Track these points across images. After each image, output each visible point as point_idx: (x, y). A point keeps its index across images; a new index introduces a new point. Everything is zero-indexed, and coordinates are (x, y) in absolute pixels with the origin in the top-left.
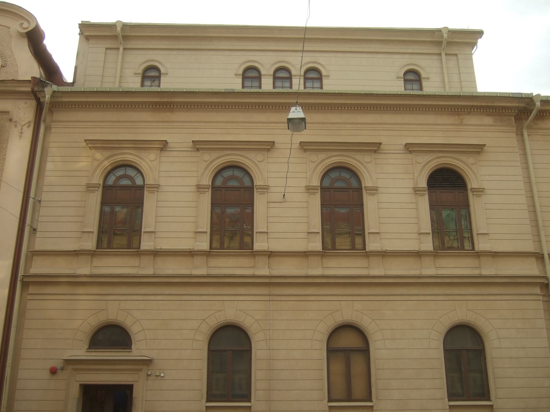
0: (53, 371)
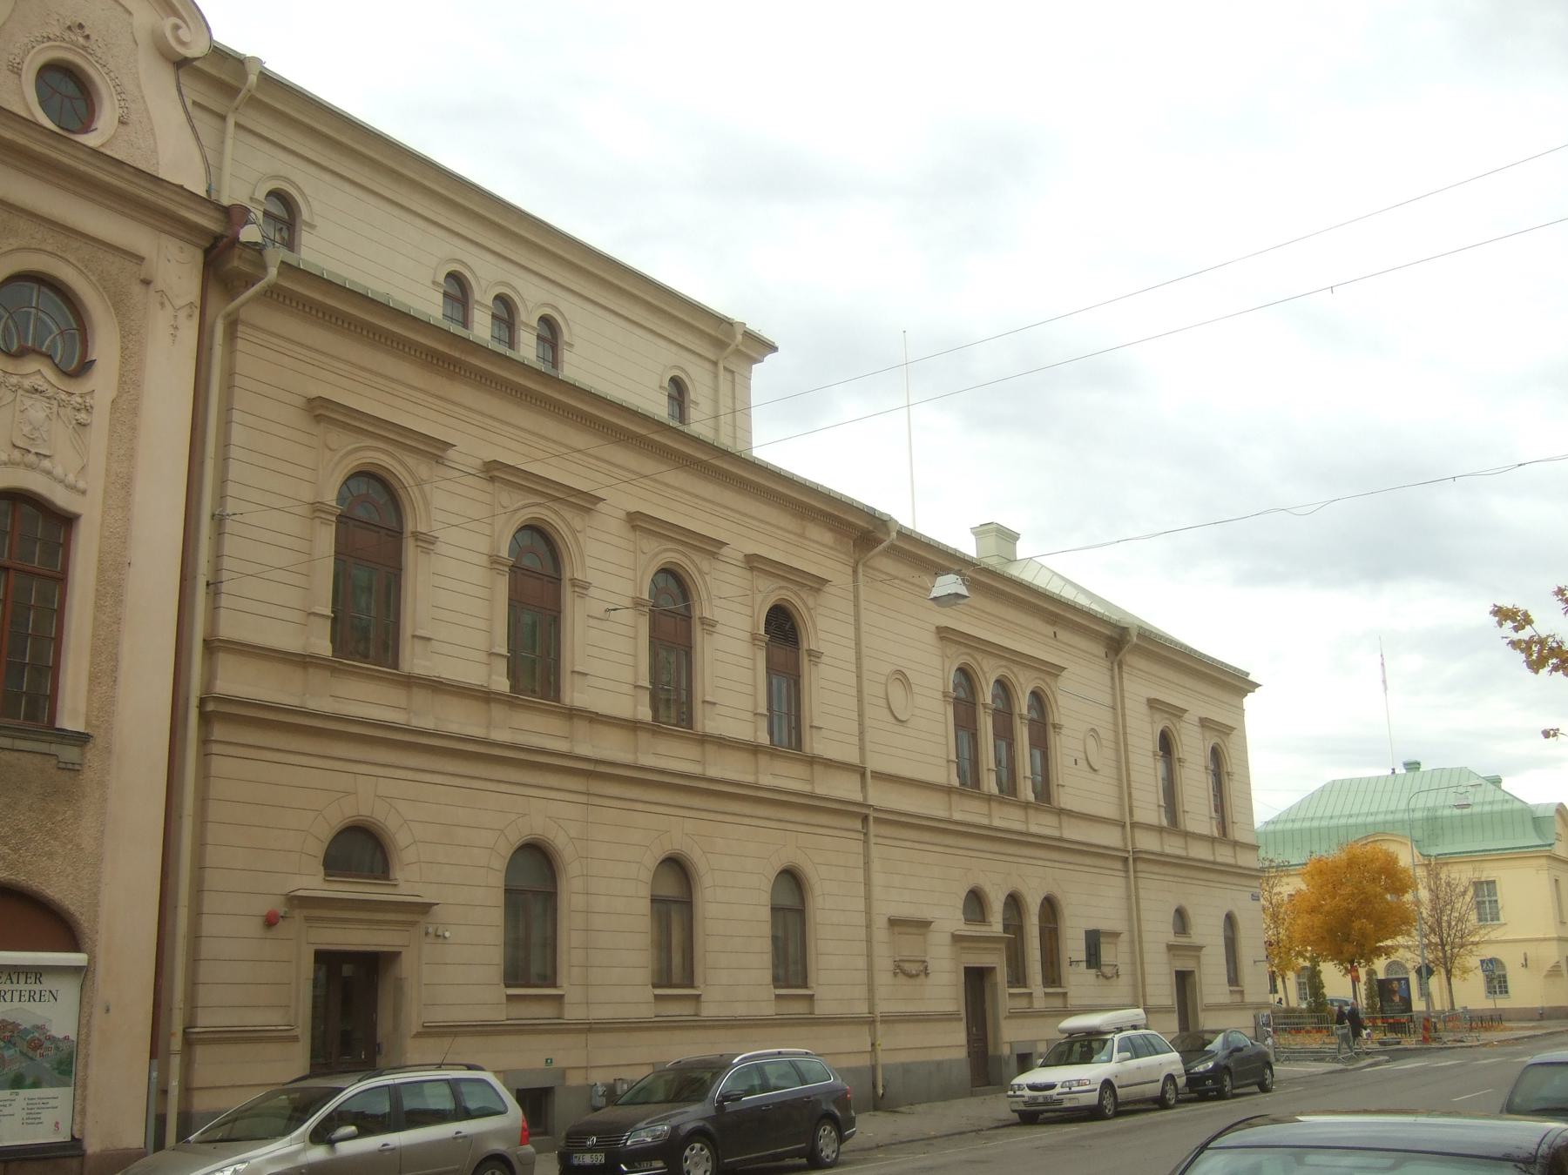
0: (271, 921)
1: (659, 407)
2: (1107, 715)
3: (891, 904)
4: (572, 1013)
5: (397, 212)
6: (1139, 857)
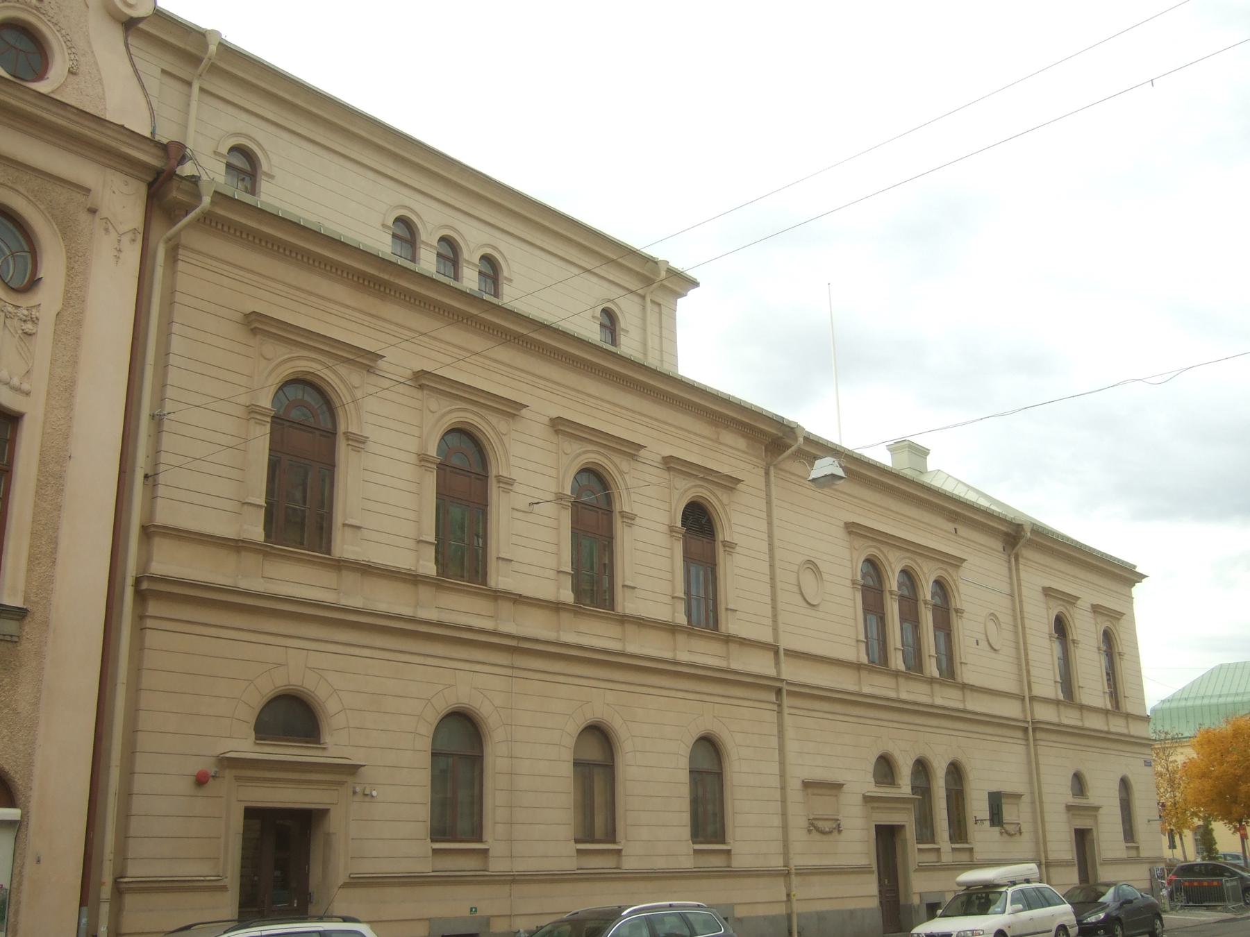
0: (201, 780)
1: (592, 332)
2: (1006, 602)
3: (805, 767)
4: (497, 866)
5: (349, 165)
6: (1038, 727)
